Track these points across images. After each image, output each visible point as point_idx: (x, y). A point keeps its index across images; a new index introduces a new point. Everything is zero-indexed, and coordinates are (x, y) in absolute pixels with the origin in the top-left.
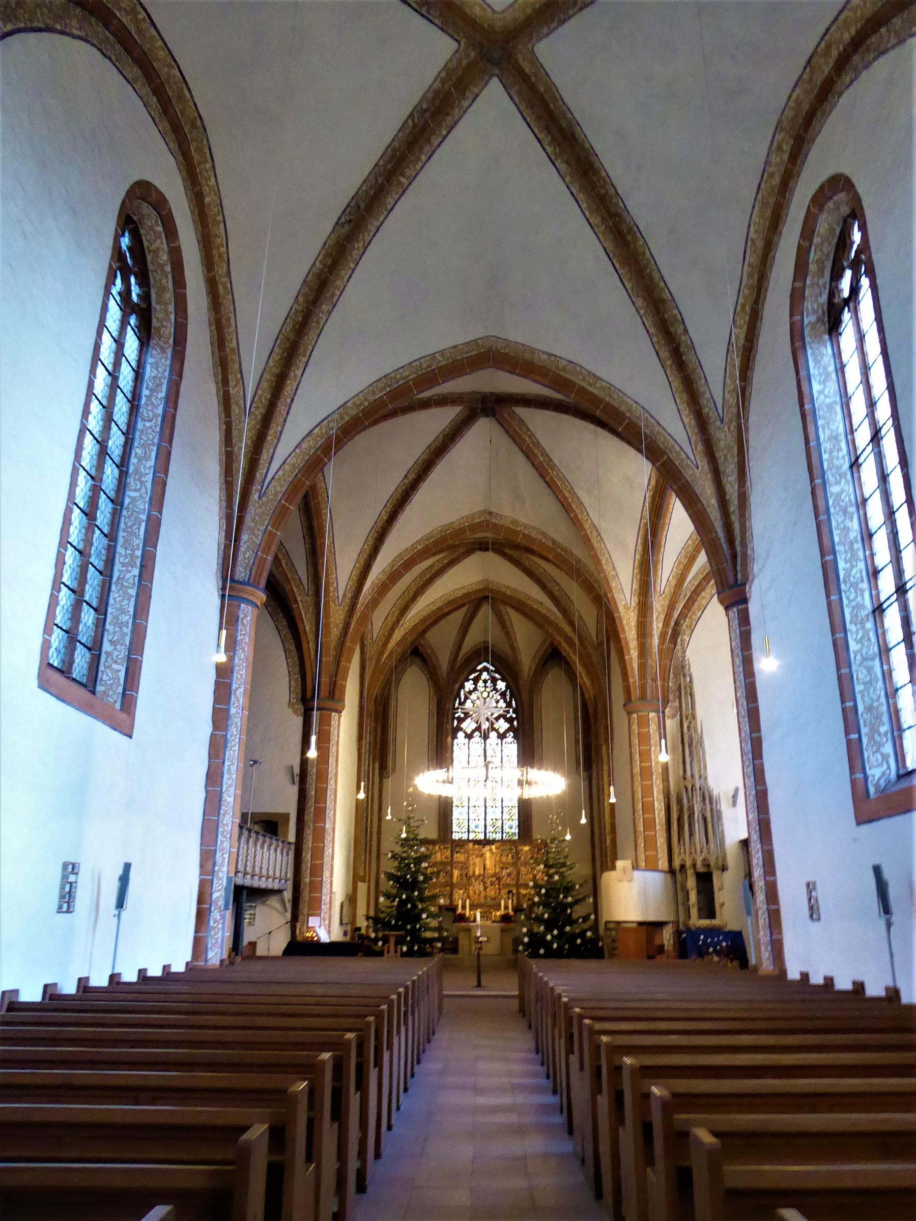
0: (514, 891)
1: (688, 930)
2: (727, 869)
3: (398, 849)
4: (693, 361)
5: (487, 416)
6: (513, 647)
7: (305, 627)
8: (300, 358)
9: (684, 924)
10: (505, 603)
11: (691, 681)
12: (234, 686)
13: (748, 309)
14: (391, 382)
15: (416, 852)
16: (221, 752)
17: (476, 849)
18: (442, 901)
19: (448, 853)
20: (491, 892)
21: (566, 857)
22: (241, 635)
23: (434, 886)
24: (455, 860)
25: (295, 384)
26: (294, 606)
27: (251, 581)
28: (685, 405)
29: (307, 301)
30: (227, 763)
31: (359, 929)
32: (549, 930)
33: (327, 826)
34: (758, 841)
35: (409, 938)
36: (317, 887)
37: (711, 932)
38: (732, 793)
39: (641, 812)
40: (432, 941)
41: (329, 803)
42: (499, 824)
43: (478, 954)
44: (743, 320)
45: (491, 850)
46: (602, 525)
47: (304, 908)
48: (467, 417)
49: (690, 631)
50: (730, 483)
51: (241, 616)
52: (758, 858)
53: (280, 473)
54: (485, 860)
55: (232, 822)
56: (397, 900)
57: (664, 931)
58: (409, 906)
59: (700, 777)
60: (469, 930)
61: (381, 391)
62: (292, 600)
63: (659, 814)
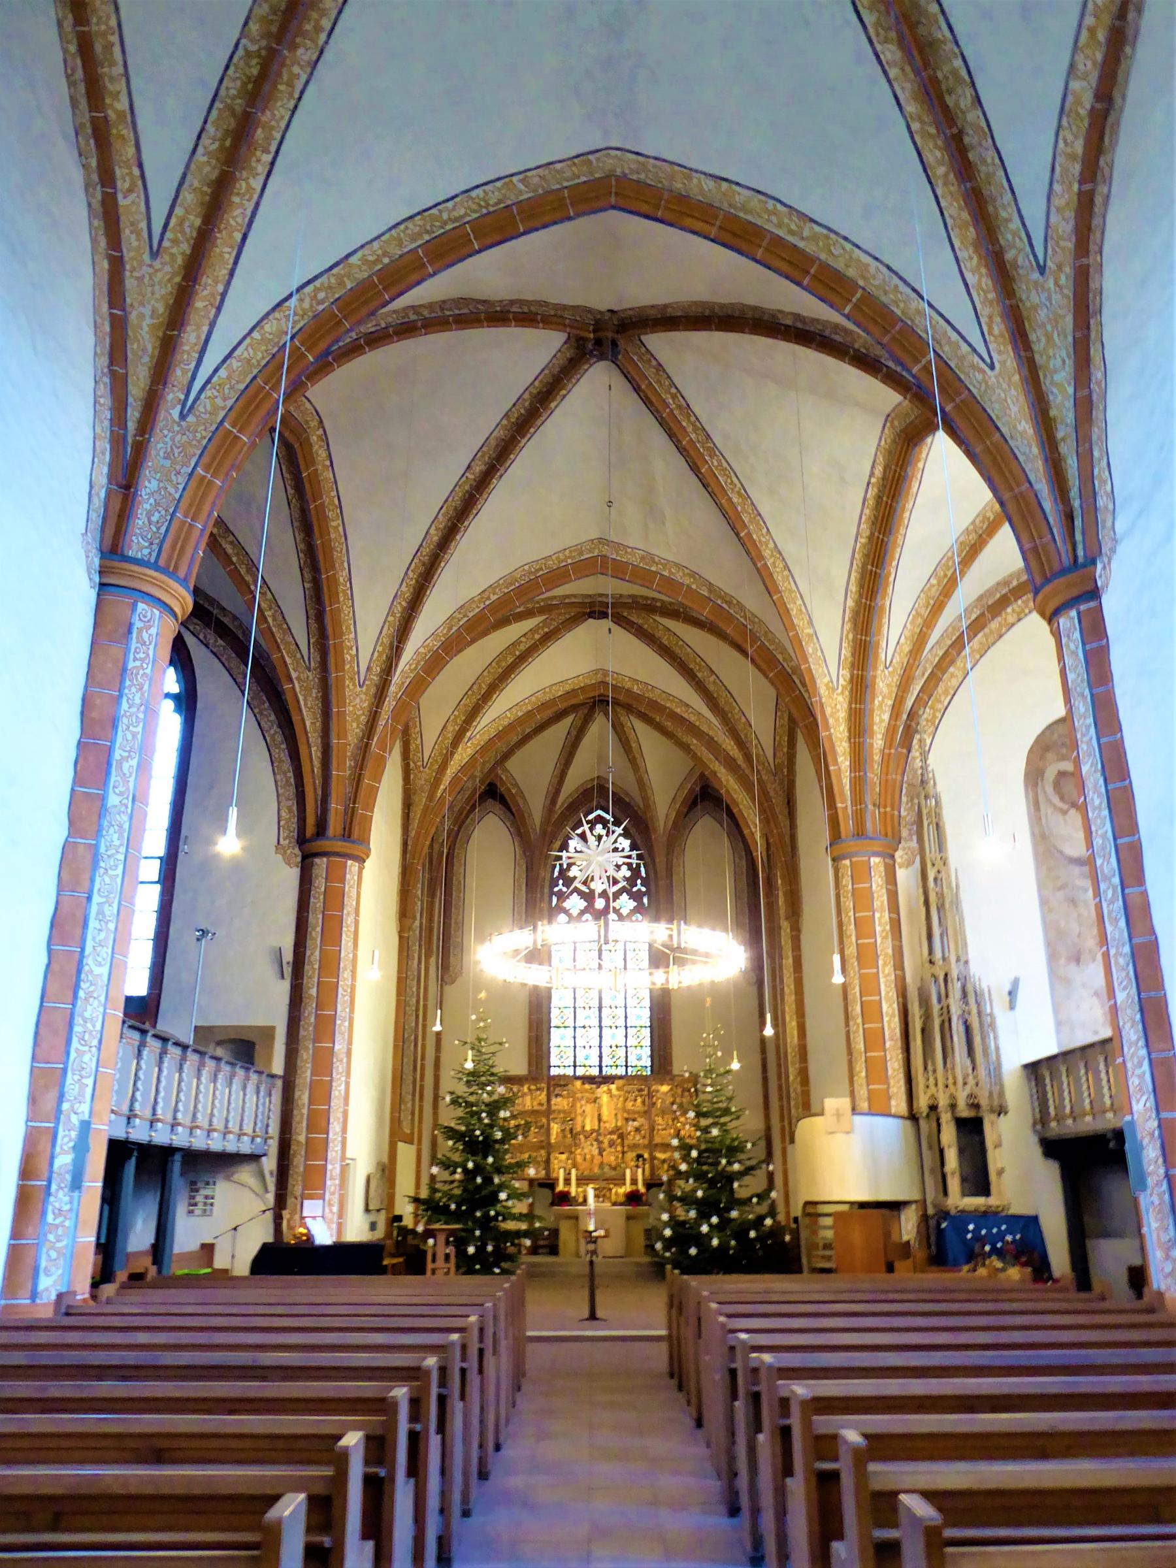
0: (646, 1156)
1: (944, 1214)
2: (1006, 1113)
3: (461, 1089)
4: (989, 160)
5: (602, 357)
6: (642, 784)
7: (303, 720)
8: (258, 153)
9: (935, 1206)
10: (629, 708)
11: (937, 803)
12: (117, 754)
13: (1101, 36)
14: (432, 226)
15: (490, 1094)
16: (85, 878)
17: (586, 1091)
18: (531, 1172)
19: (543, 1096)
20: (610, 1158)
21: (730, 1099)
22: (135, 659)
23: (521, 1148)
24: (554, 1108)
25: (250, 206)
26: (287, 687)
27: (162, 563)
28: (971, 250)
29: (267, 35)
30: (96, 899)
31: (399, 1218)
32: (704, 1216)
33: (337, 1047)
34: (1142, 1043)
35: (478, 1233)
36: (318, 1149)
37: (986, 1216)
38: (1008, 987)
39: (859, 1020)
40: (518, 1234)
41: (342, 1009)
42: (621, 1052)
43: (591, 1263)
44: (1090, 64)
45: (610, 1090)
46: (789, 548)
47: (296, 1185)
48: (571, 360)
49: (932, 729)
50: (1057, 385)
51: (138, 624)
52: (1141, 1077)
53: (223, 373)
54: (599, 1108)
55: (104, 1014)
56: (459, 1170)
57: (903, 1217)
58: (479, 1180)
59: (958, 960)
60: (575, 1218)
61: (413, 240)
62: (283, 679)
63: (889, 1022)
